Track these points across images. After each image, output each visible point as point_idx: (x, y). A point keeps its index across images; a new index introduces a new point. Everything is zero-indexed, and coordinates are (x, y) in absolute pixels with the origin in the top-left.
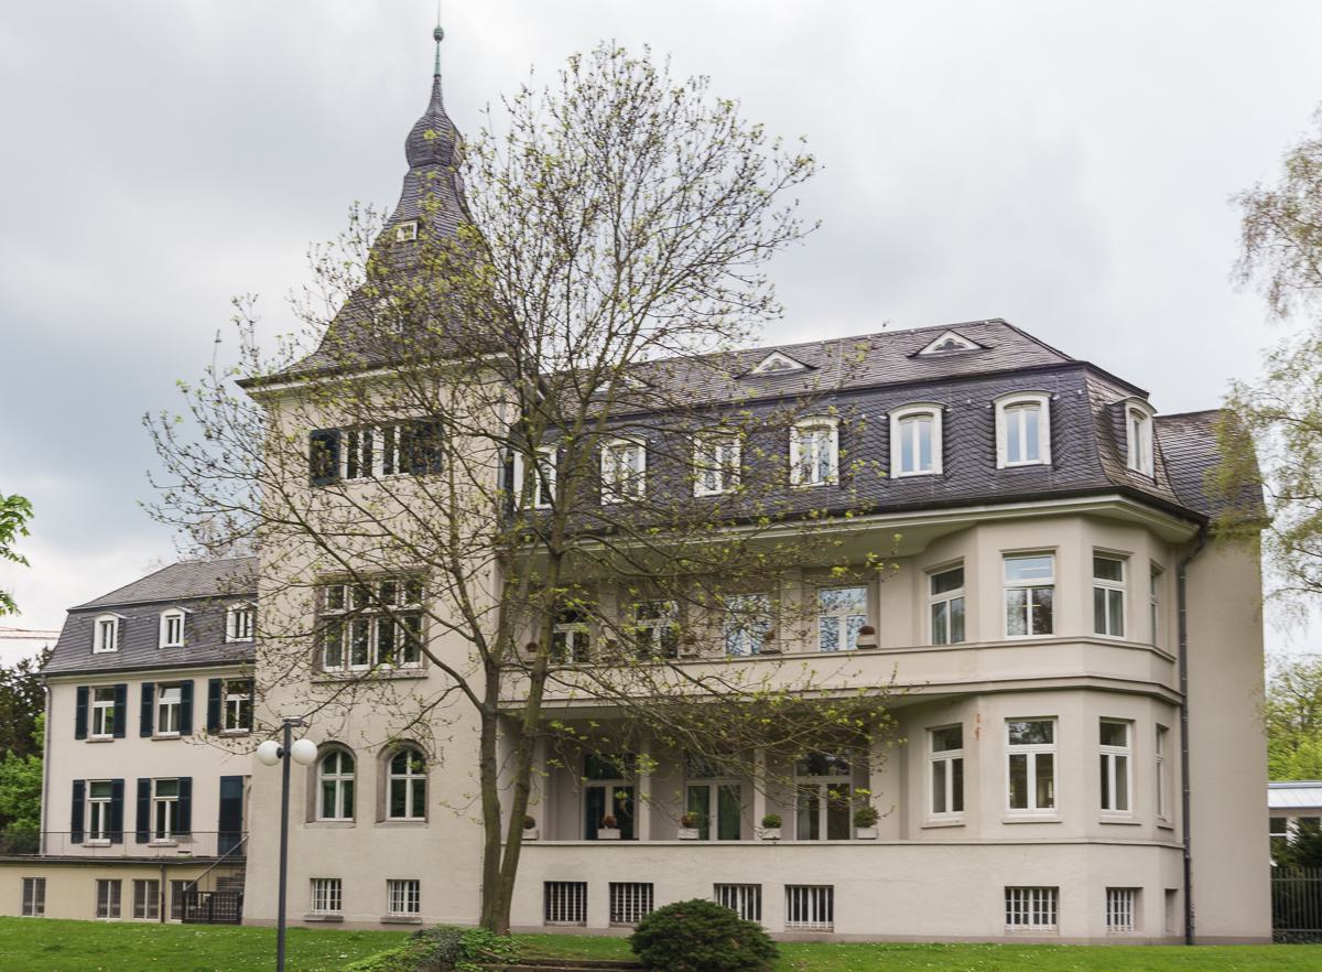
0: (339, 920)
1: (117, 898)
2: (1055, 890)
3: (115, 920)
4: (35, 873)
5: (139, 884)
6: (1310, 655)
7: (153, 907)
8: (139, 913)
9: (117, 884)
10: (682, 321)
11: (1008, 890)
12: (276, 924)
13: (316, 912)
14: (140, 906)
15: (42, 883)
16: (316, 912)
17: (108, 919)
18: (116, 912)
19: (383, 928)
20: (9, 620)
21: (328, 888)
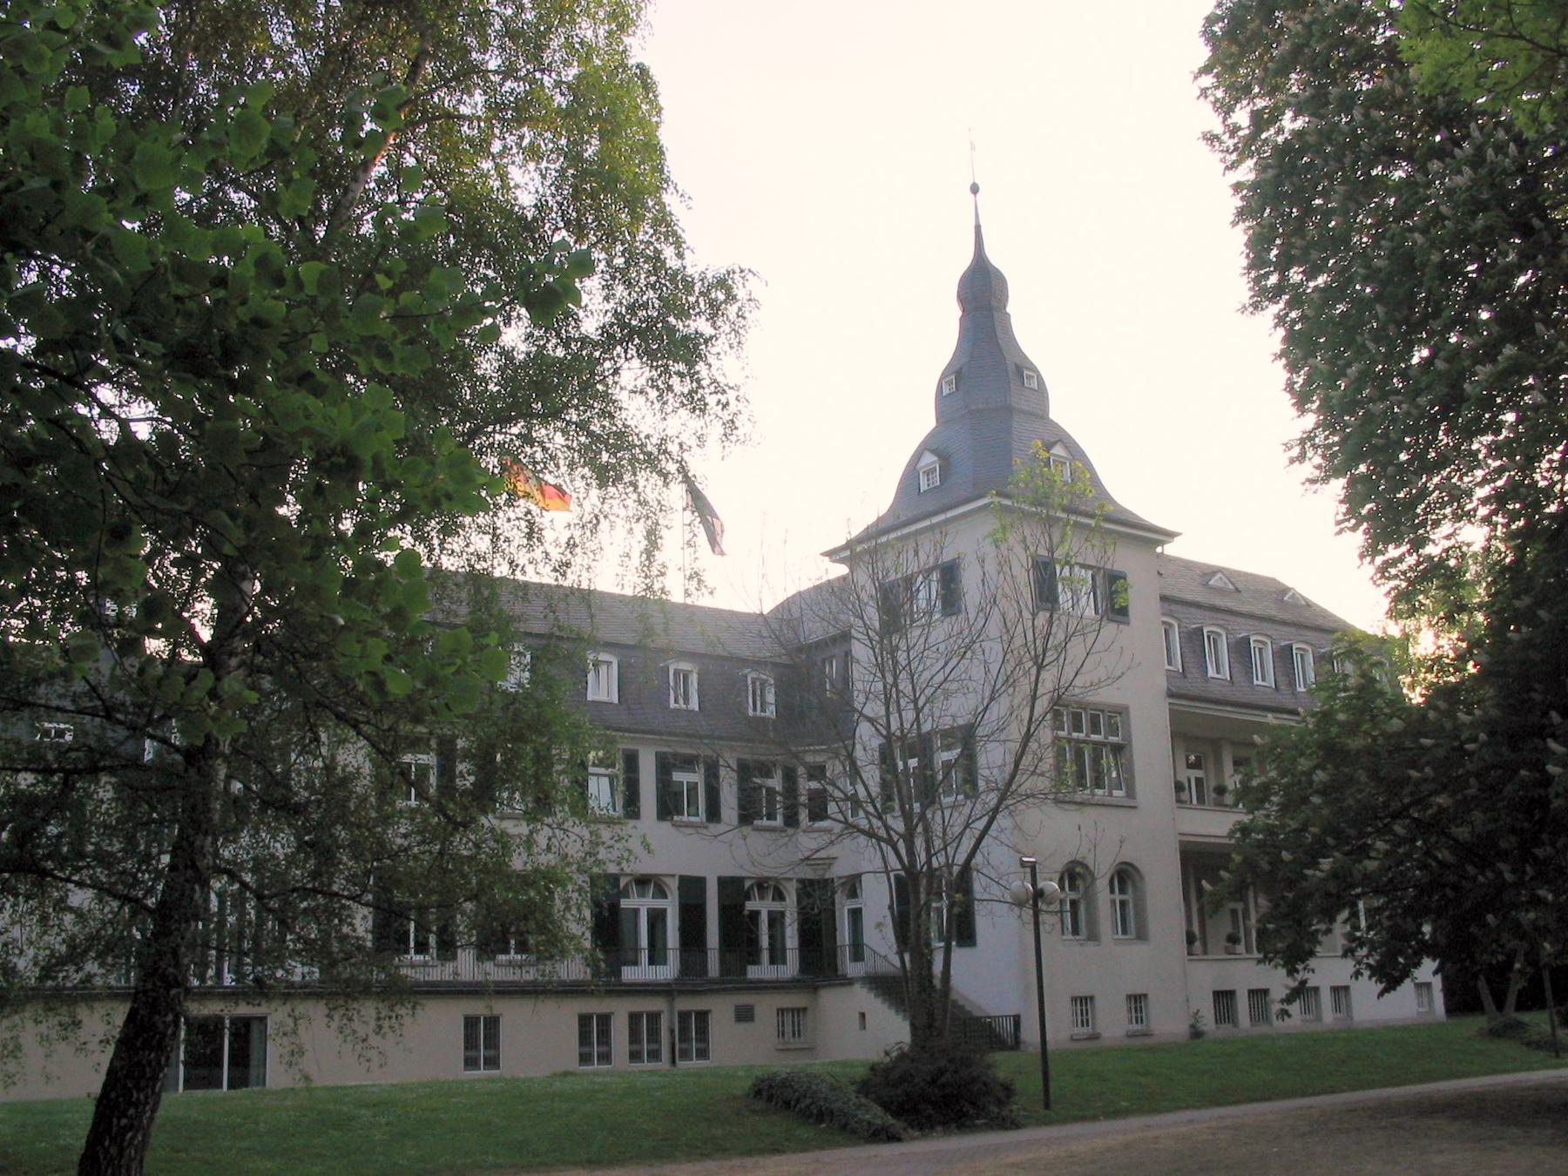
0: (1146, 1035)
1: (654, 1035)
2: (1092, 998)
3: (702, 1063)
4: (745, 999)
5: (634, 1018)
6: (1081, 804)
7: (684, 1046)
8: (635, 1056)
9: (605, 1020)
10: (160, 516)
11: (1129, 997)
12: (1039, 1050)
13: (1076, 1030)
14: (702, 1045)
15: (493, 1023)
16: (1076, 1030)
17: (482, 1072)
18: (605, 1057)
19: (1126, 1042)
20: (18, 729)
21: (1083, 1003)
